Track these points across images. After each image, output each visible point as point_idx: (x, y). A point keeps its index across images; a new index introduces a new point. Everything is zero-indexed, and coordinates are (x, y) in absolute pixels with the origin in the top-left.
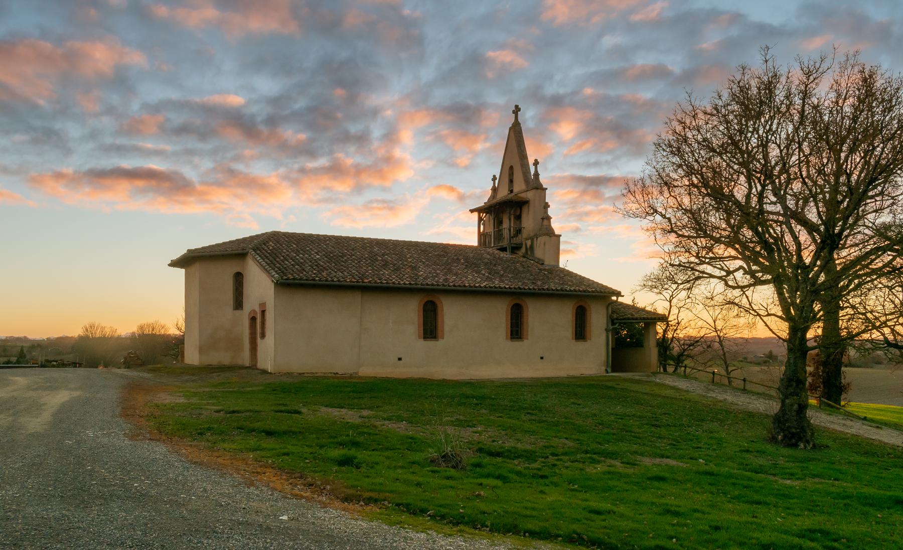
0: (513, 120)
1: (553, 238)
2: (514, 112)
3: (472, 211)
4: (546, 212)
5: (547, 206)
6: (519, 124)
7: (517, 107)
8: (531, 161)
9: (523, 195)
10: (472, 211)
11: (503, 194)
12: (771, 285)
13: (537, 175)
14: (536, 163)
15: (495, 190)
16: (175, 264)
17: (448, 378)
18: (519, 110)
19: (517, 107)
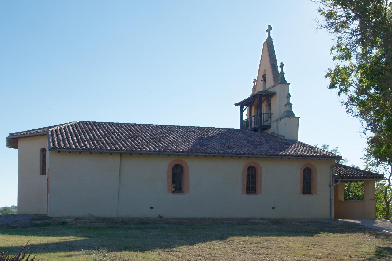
0: (267, 37)
1: (293, 119)
2: (267, 31)
3: (236, 105)
4: (289, 100)
5: (289, 96)
6: (271, 39)
7: (269, 27)
8: (279, 65)
9: (272, 90)
10: (236, 105)
11: (260, 89)
12: (239, 128)
13: (282, 73)
14: (282, 65)
15: (254, 88)
16: (13, 141)
17: (331, 235)
18: (271, 28)
19: (269, 27)
